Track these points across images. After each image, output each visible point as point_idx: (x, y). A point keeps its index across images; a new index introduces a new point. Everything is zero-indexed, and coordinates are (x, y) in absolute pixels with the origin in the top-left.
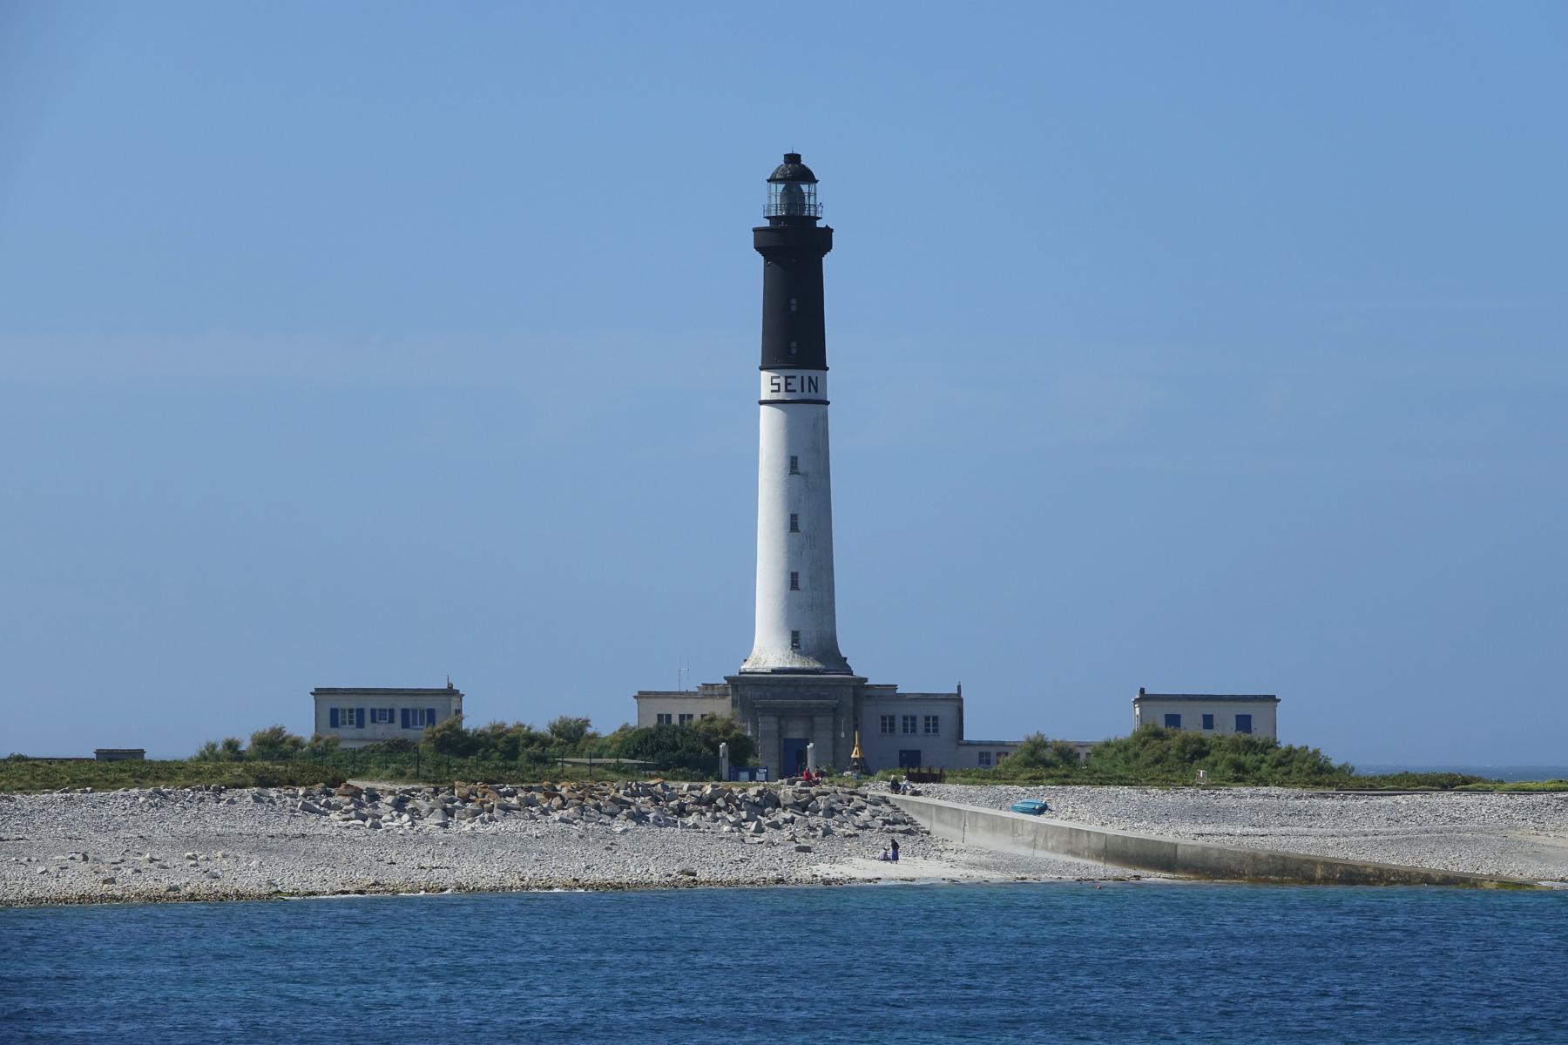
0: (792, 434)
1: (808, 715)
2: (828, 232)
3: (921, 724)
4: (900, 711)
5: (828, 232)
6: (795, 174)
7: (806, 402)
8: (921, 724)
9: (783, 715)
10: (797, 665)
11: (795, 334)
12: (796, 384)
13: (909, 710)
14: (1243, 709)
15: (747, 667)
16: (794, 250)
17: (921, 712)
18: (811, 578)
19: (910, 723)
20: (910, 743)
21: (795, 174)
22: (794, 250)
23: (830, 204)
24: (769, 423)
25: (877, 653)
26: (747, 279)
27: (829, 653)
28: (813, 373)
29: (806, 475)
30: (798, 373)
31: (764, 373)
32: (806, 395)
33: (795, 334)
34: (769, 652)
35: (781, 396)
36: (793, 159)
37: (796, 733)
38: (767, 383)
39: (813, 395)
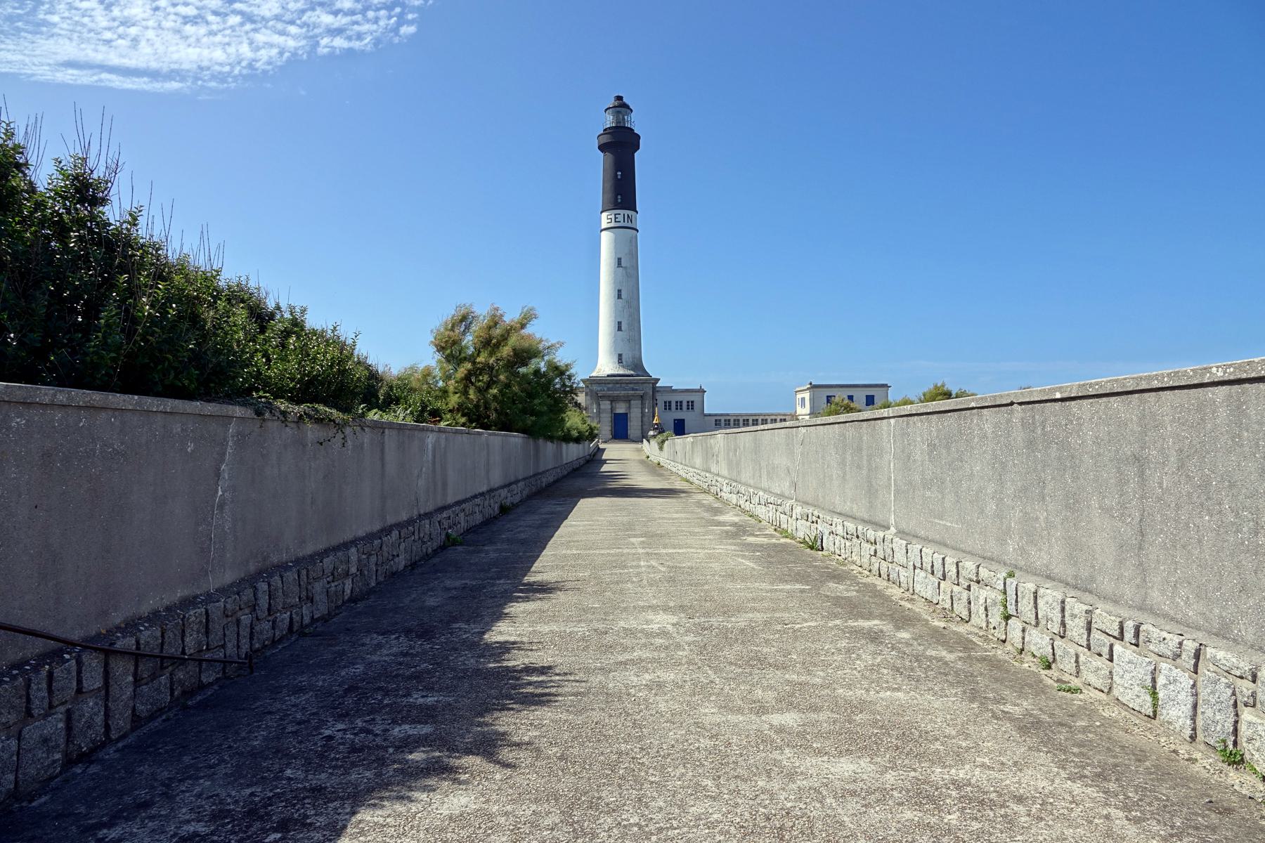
0: (617, 243)
1: (628, 400)
2: (515, 687)
3: (685, 405)
4: (674, 398)
5: (515, 687)
6: (621, 106)
7: (626, 228)
8: (685, 405)
9: (613, 400)
10: (621, 372)
11: (622, 194)
12: (620, 218)
13: (679, 398)
14: (870, 392)
15: (594, 374)
16: (621, 145)
17: (685, 398)
18: (628, 326)
19: (679, 405)
20: (679, 415)
21: (621, 106)
22: (621, 145)
23: (636, 122)
24: (606, 239)
25: (667, 370)
26: (596, 165)
27: (638, 366)
28: (630, 213)
29: (625, 268)
30: (622, 212)
31: (604, 215)
32: (626, 224)
33: (622, 194)
34: (605, 366)
35: (612, 225)
36: (619, 98)
37: (621, 409)
38: (605, 219)
39: (629, 225)
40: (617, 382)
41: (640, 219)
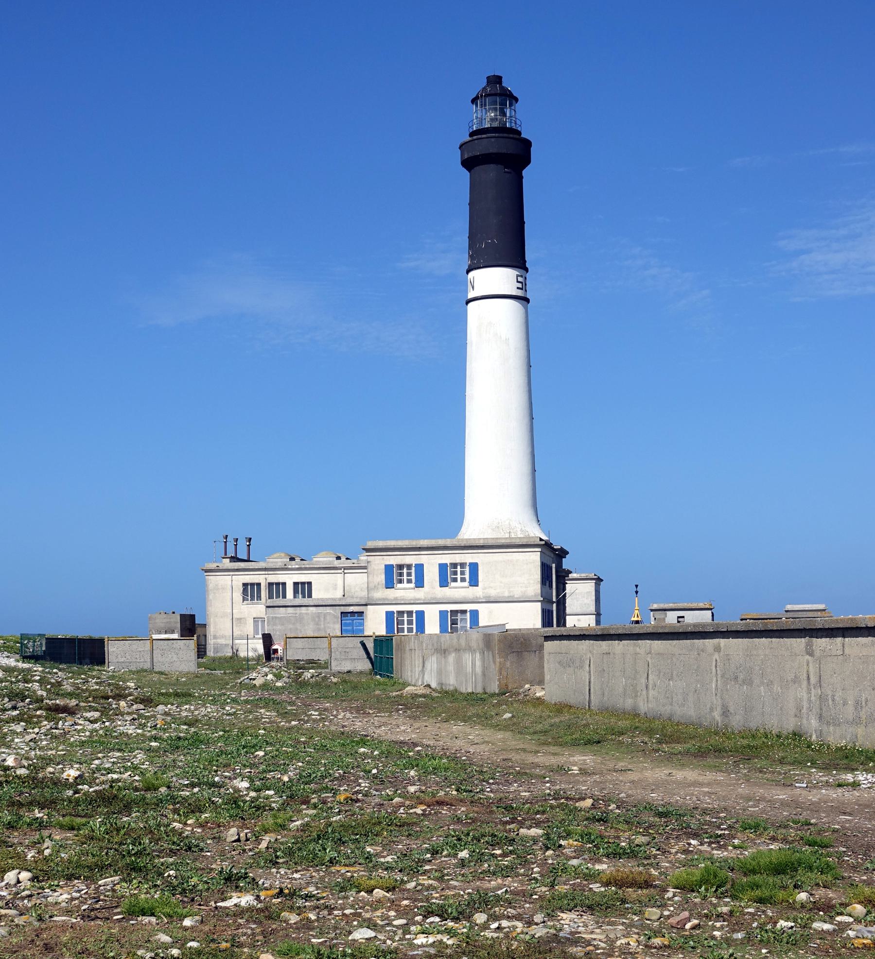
6: (497, 93)
16: (499, 160)
22: (499, 160)
23: (526, 119)
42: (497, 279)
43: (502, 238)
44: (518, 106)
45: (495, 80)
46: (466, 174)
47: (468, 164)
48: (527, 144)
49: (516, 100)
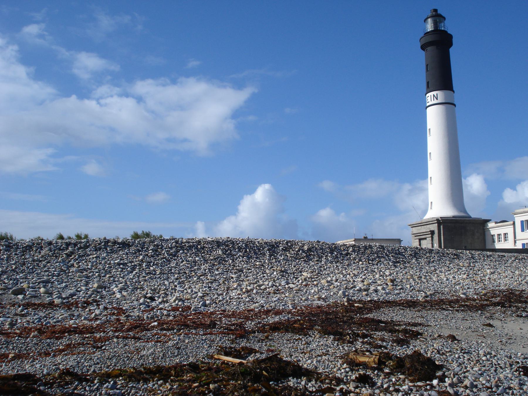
6: (437, 17)
16: (439, 44)
22: (439, 44)
23: (448, 26)
28: (449, 92)
40: (456, 220)
41: (457, 96)
42: (439, 95)
43: (442, 78)
44: (446, 22)
45: (436, 10)
46: (423, 53)
47: (423, 47)
48: (450, 37)
49: (444, 18)
